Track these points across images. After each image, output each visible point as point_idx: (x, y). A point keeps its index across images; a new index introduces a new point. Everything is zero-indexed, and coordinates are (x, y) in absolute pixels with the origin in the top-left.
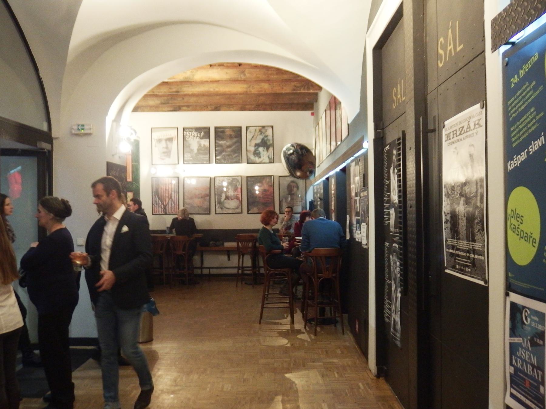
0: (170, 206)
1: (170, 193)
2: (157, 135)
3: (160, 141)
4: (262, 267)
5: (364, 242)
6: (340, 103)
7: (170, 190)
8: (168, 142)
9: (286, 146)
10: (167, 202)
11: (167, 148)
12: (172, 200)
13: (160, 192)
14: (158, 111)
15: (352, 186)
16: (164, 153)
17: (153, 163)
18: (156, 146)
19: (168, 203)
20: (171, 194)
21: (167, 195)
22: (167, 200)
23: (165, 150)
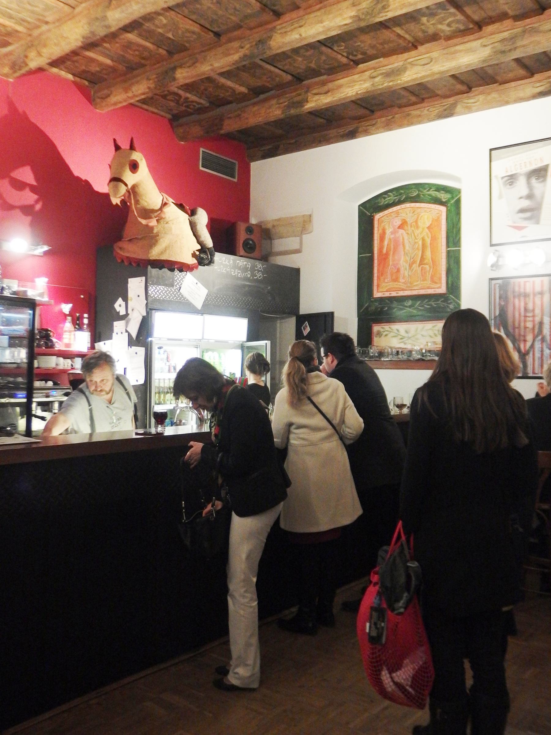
0: (538, 355)
1: (537, 319)
2: (505, 165)
3: (511, 179)
4: (32, 356)
5: (264, 355)
6: (213, 263)
7: (538, 311)
8: (533, 181)
9: (103, 346)
10: (529, 344)
11: (530, 196)
12: (543, 340)
13: (510, 321)
14: (507, 103)
15: (256, 603)
16: (522, 211)
17: (493, 152)
18: (500, 197)
19: (532, 346)
20: (541, 324)
21: (529, 325)
22: (530, 338)
23: (526, 203)
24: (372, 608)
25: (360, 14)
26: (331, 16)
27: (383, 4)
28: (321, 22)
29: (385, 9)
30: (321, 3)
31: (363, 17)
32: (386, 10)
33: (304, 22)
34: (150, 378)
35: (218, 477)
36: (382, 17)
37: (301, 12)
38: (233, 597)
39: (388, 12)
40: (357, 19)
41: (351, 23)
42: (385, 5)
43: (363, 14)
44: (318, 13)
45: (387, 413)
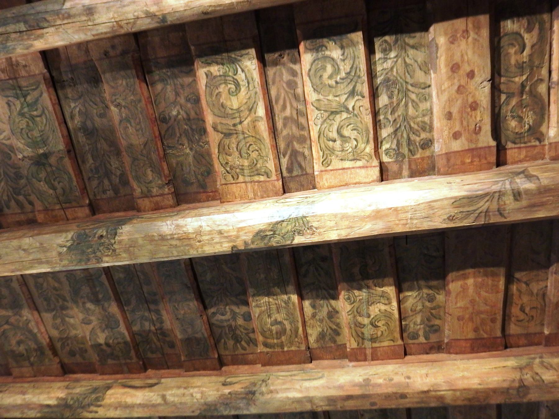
24: (451, 189)
25: (70, 398)
26: (38, 391)
27: (98, 395)
28: (24, 393)
29: (99, 401)
30: (35, 376)
31: (71, 403)
32: (99, 403)
33: (5, 389)
34: (372, 102)
35: (292, 69)
36: (91, 412)
37: (10, 379)
38: (349, 234)
39: (100, 406)
40: (64, 402)
41: (55, 406)
42: (100, 397)
43: (72, 399)
44: (26, 385)
45: (554, 344)
